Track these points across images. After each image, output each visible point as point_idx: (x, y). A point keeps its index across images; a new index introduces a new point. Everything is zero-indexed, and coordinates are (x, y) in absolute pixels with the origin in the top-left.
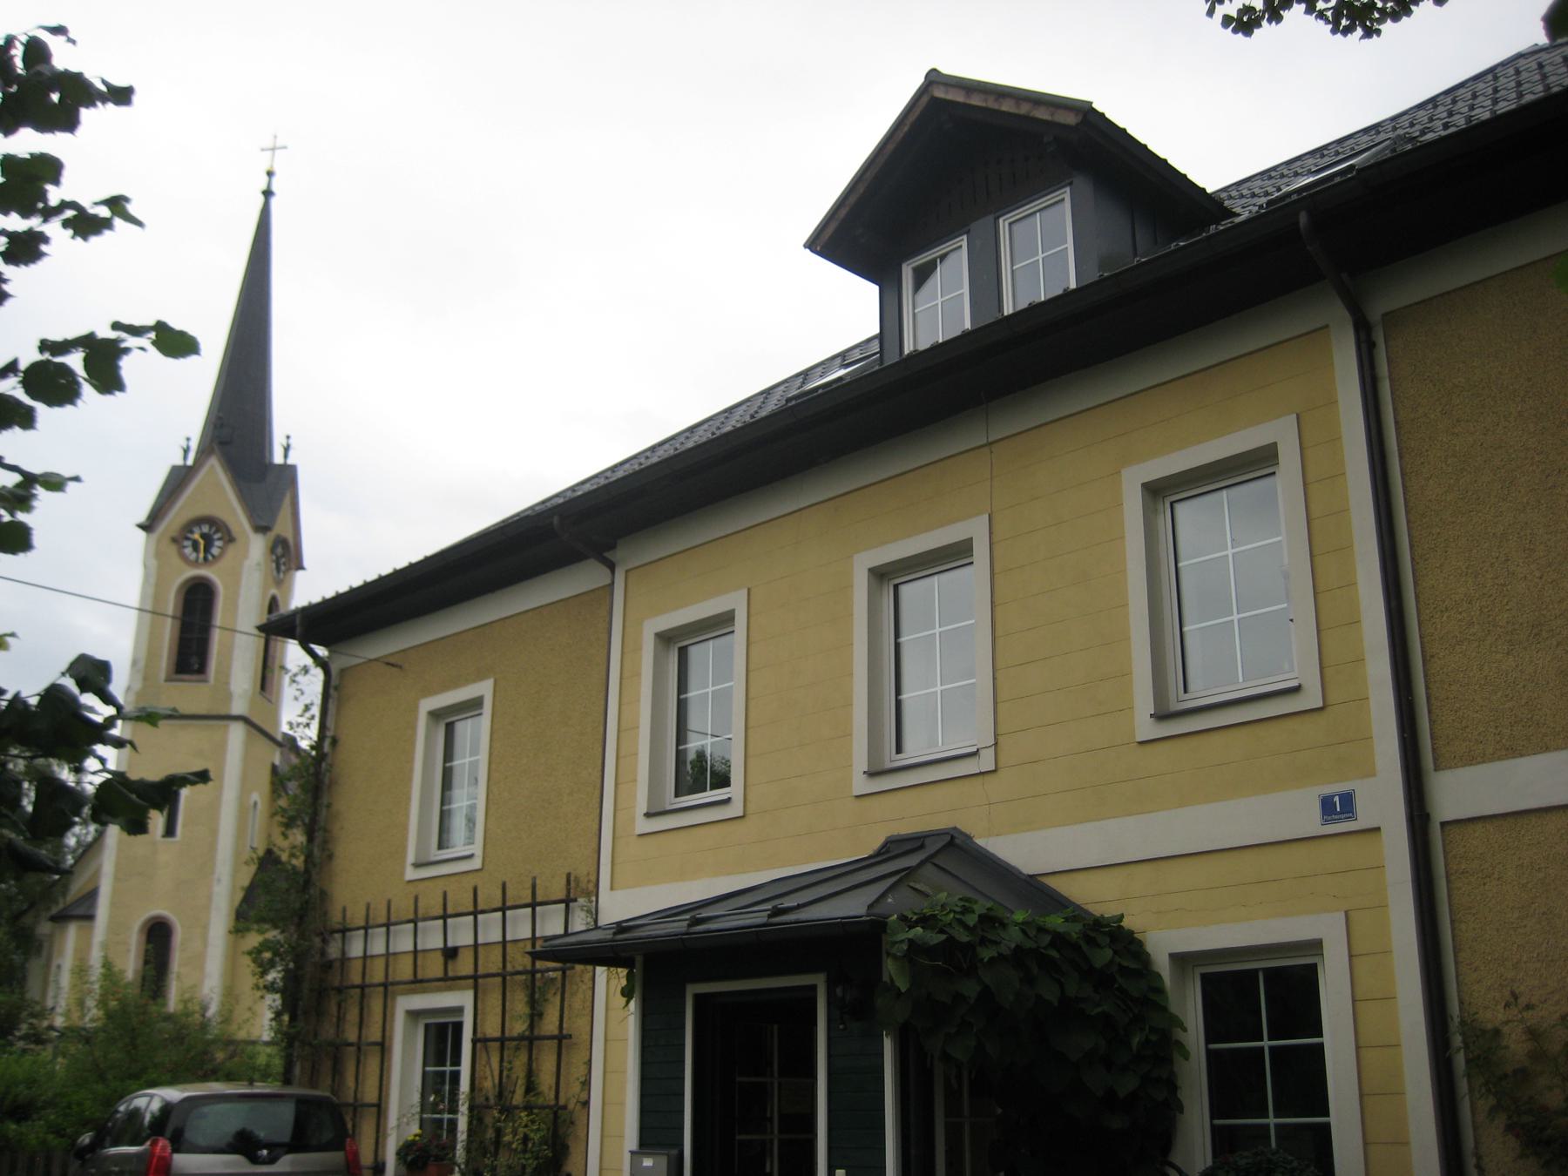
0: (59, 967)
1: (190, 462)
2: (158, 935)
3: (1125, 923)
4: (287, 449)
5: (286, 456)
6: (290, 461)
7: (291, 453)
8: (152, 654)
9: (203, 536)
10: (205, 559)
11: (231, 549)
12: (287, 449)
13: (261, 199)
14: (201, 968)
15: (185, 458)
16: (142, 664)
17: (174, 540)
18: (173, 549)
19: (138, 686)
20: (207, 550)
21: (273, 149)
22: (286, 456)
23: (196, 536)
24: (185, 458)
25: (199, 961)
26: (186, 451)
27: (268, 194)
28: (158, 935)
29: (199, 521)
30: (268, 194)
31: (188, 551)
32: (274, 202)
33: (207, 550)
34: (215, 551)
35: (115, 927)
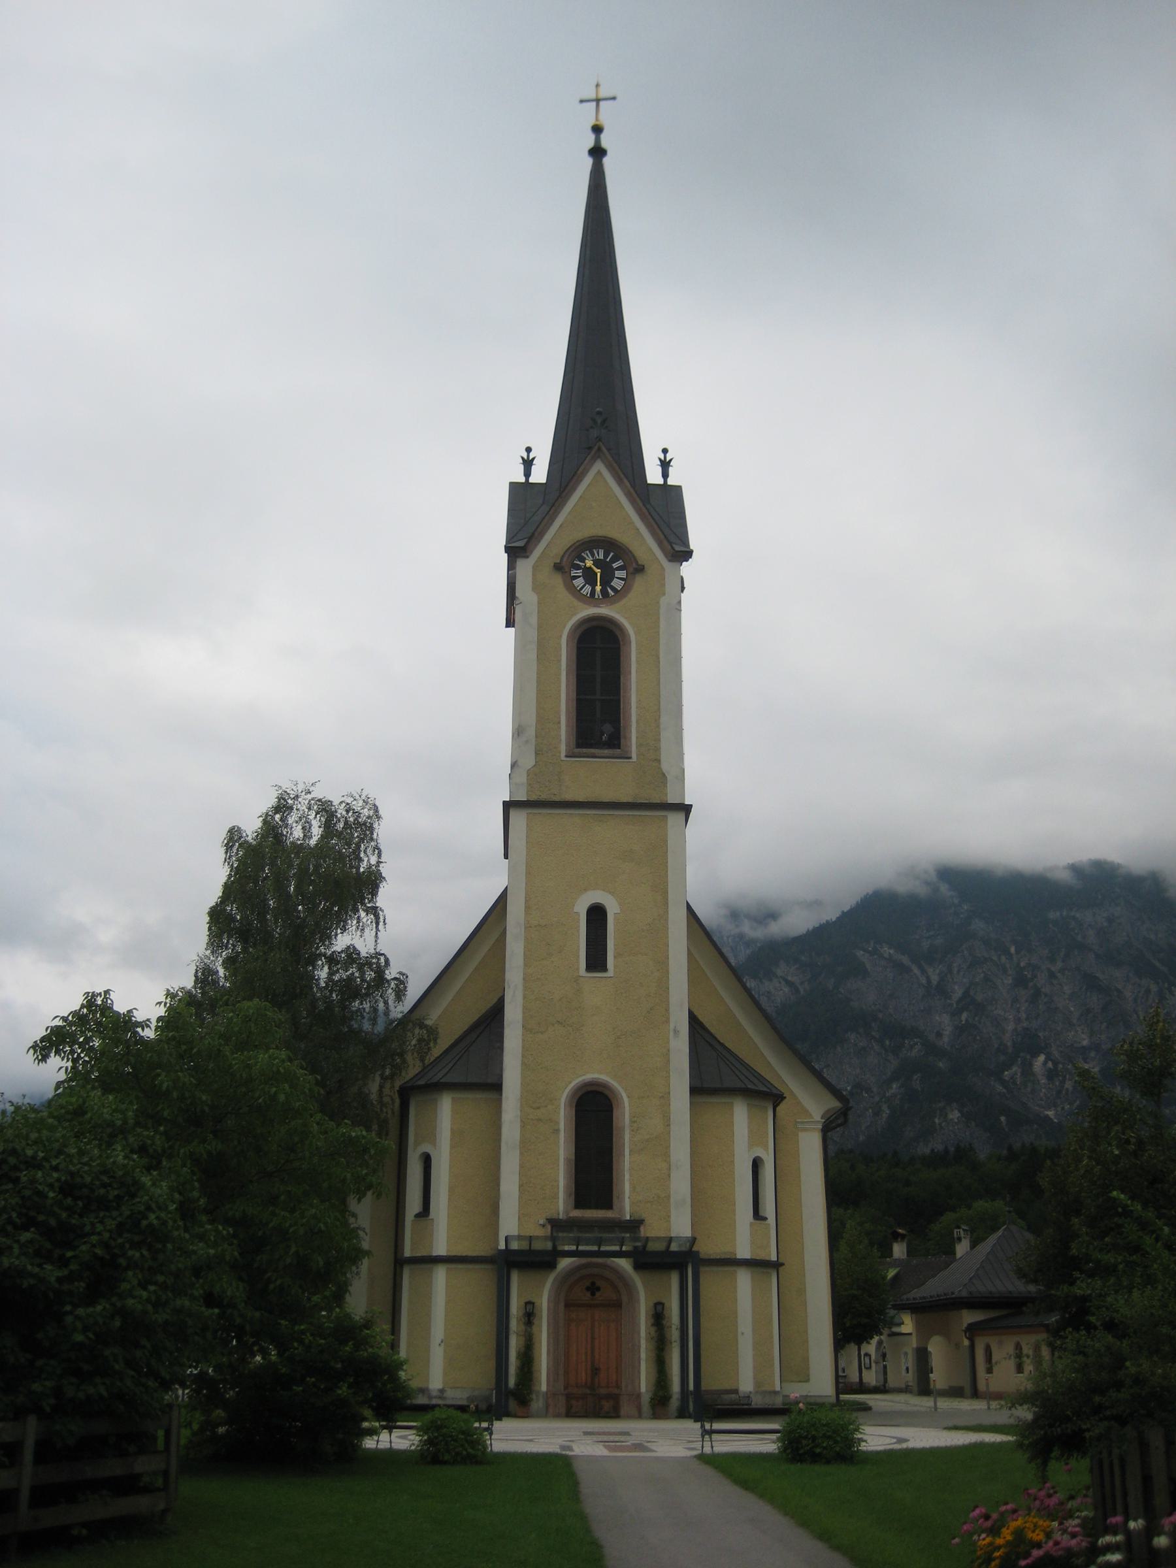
0: (427, 1160)
1: (539, 475)
2: (594, 1111)
3: (347, 1295)
4: (665, 465)
5: (665, 475)
6: (671, 481)
7: (671, 471)
8: (544, 720)
9: (597, 563)
10: (604, 593)
11: (639, 582)
12: (665, 465)
13: (589, 161)
14: (666, 1155)
15: (527, 474)
16: (531, 732)
17: (558, 567)
18: (558, 580)
19: (529, 761)
20: (606, 582)
21: (598, 101)
22: (665, 475)
23: (589, 563)
24: (527, 474)
25: (660, 1145)
26: (528, 464)
27: (598, 152)
28: (594, 1111)
29: (592, 544)
30: (598, 152)
31: (579, 582)
32: (607, 161)
33: (606, 582)
34: (617, 584)
35: (532, 1099)
